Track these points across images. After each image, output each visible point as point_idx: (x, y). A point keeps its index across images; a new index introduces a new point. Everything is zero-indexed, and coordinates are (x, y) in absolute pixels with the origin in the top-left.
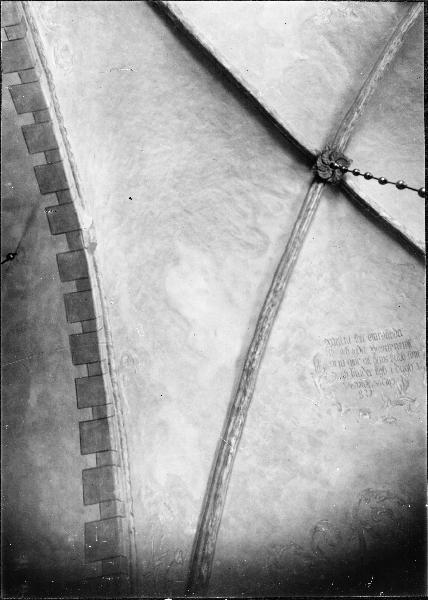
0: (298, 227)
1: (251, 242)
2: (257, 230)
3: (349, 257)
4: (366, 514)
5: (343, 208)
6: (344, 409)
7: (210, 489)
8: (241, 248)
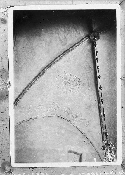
0: (76, 45)
1: (62, 40)
2: (66, 38)
3: (82, 58)
4: (45, 30)
5: (89, 47)
6: (59, 86)
7: (22, 92)
8: (59, 41)
